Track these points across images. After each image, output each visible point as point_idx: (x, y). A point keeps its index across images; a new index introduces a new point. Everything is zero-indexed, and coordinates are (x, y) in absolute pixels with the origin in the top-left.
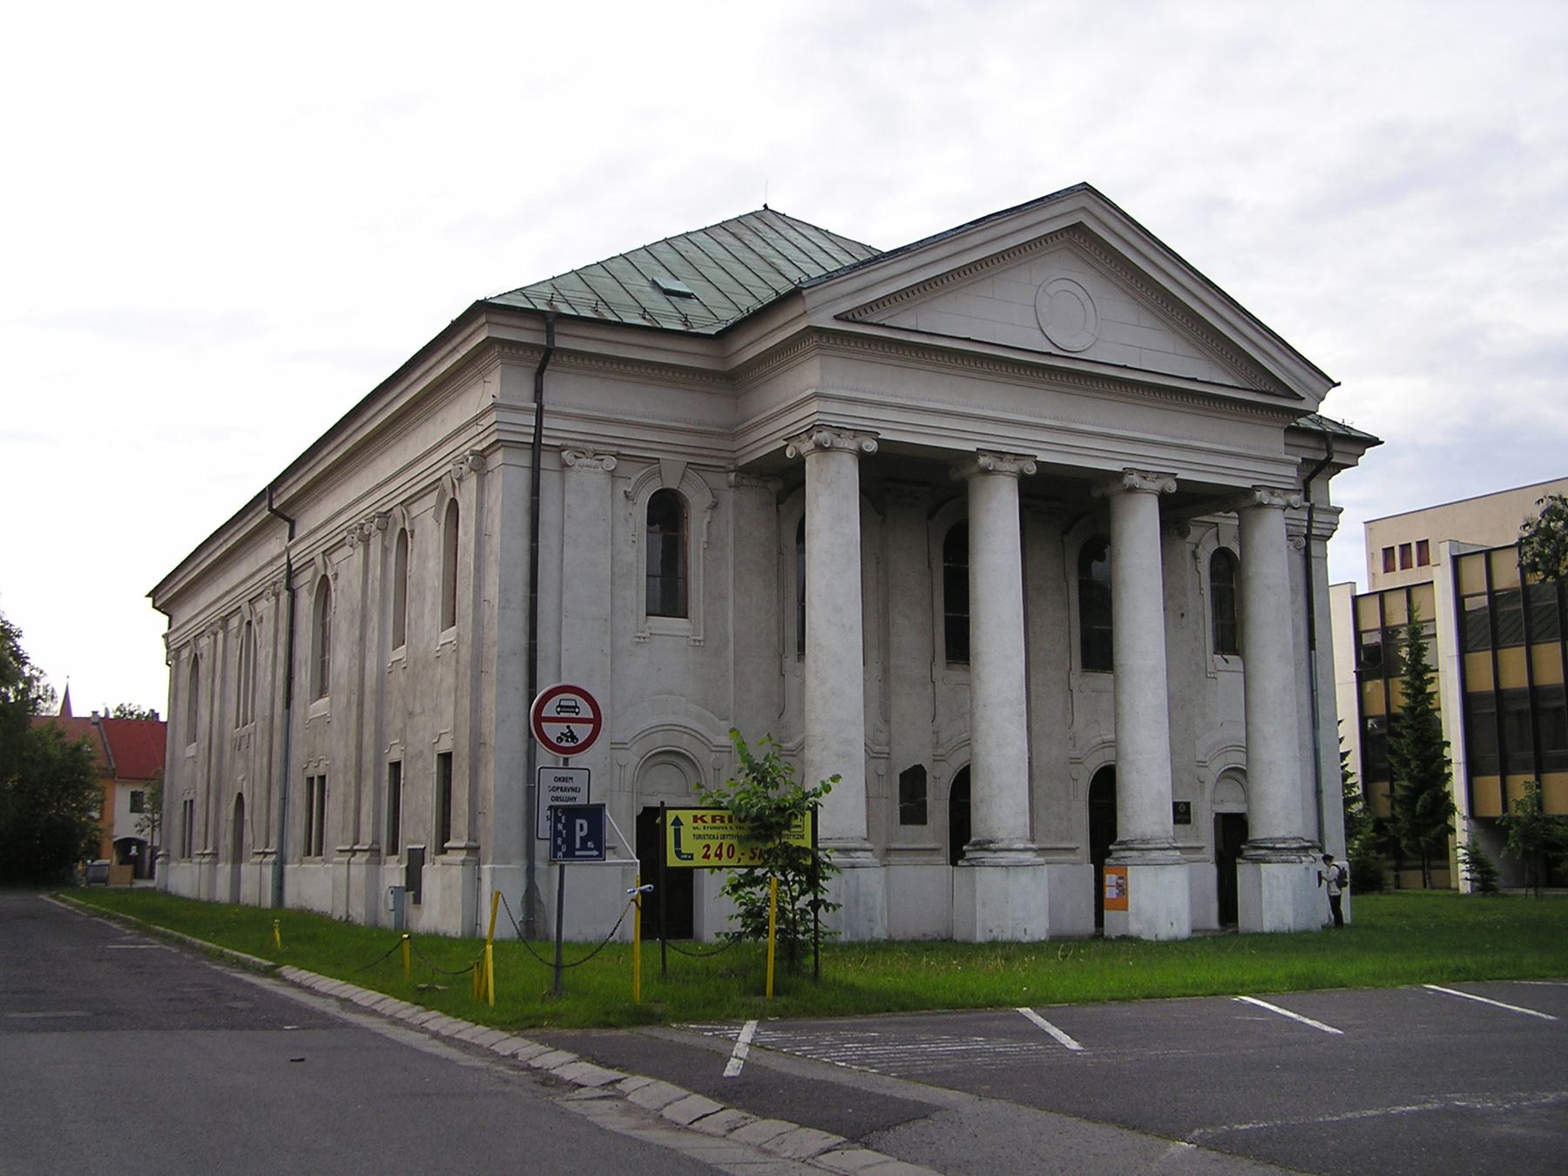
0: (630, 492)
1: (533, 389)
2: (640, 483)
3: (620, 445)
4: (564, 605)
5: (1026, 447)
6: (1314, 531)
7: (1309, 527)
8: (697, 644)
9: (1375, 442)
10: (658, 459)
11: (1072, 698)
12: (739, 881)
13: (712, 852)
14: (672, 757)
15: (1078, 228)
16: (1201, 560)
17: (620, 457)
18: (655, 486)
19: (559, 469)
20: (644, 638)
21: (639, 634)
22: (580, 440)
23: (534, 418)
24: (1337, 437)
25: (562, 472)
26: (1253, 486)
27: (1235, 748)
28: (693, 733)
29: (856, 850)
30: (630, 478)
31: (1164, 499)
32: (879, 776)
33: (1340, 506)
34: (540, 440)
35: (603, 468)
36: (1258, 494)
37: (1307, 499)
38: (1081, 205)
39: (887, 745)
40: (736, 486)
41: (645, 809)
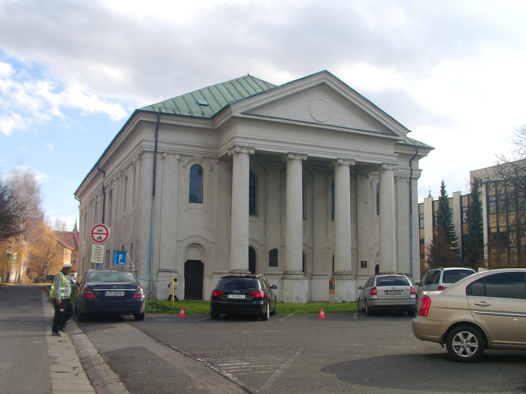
1: (155, 135)
2: (189, 162)
3: (181, 152)
6: (413, 177)
7: (411, 176)
10: (193, 156)
12: (16, 269)
14: (195, 245)
15: (323, 84)
20: (188, 209)
21: (186, 208)
22: (169, 150)
26: (382, 163)
30: (184, 161)
37: (410, 167)
39: (266, 242)
40: (218, 163)
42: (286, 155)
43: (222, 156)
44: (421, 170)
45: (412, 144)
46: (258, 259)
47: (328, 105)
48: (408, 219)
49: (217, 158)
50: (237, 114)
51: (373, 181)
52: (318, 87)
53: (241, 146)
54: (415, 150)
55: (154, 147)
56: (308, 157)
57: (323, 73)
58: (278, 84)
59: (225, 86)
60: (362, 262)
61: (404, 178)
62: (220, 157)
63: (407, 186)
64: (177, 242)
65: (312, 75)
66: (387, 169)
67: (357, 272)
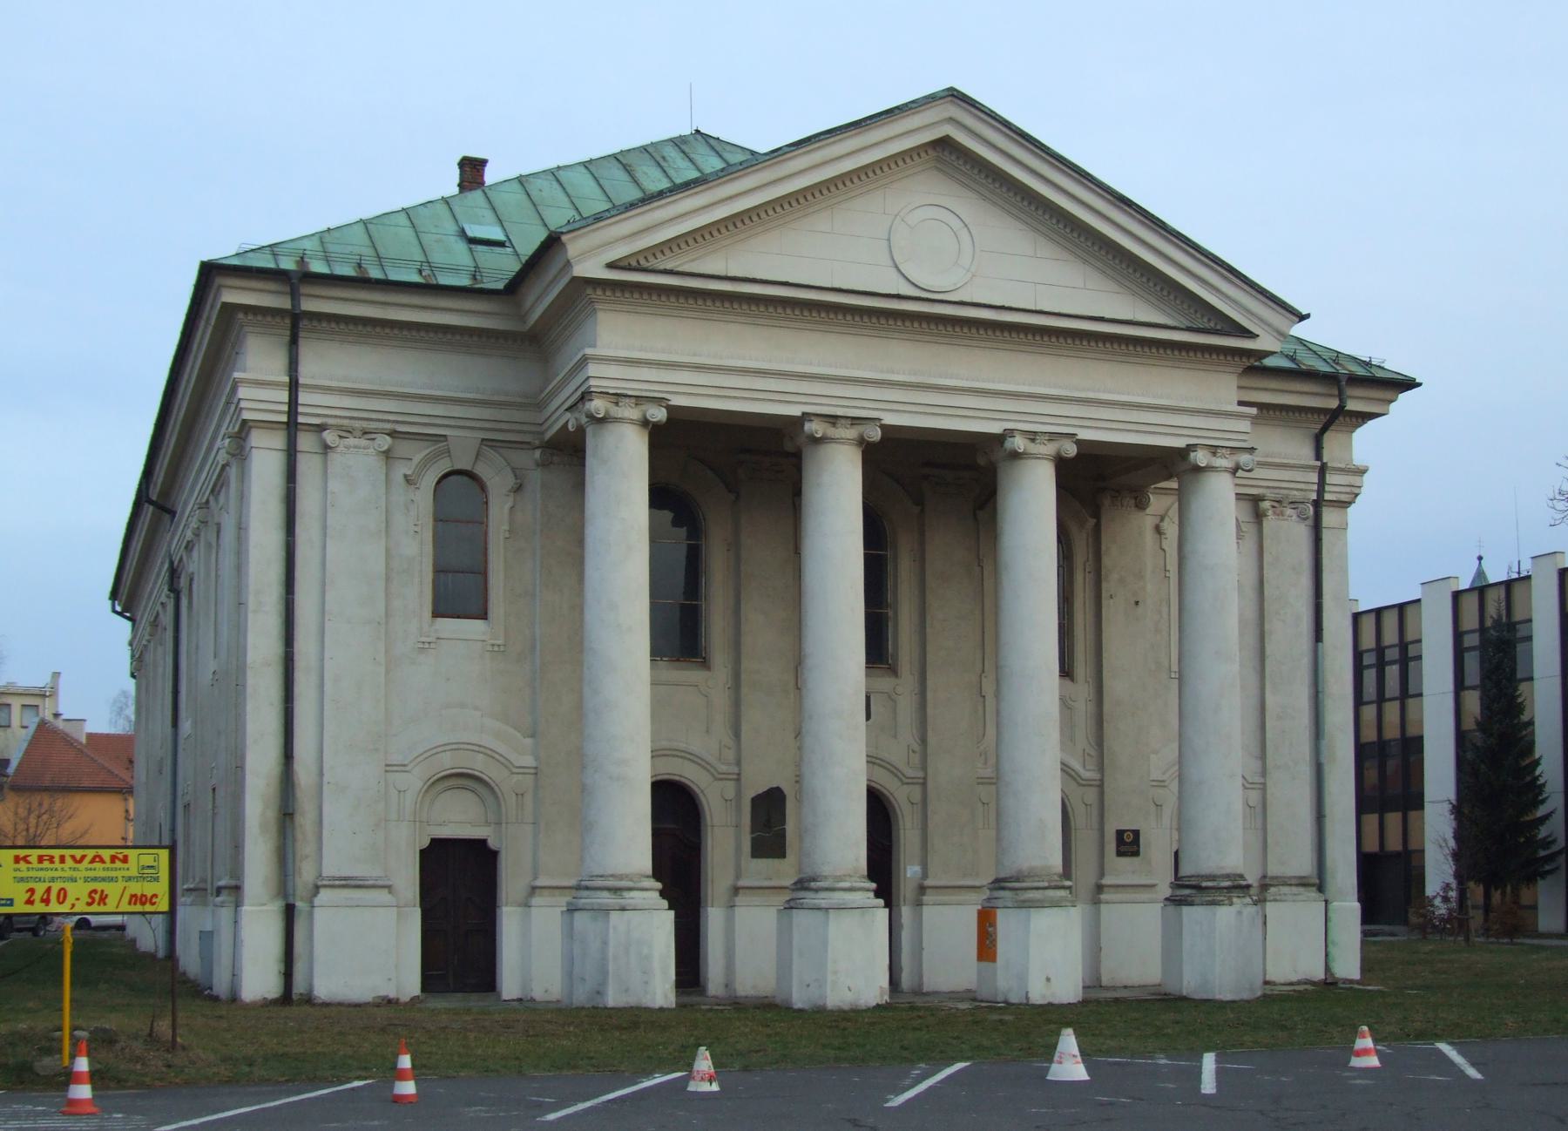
0: (410, 476)
3: (397, 422)
4: (327, 608)
5: (869, 409)
6: (1327, 497)
8: (496, 649)
9: (1408, 384)
10: (445, 436)
11: (984, 706)
13: (37, 897)
14: (465, 779)
15: (944, 144)
16: (1167, 536)
17: (394, 435)
18: (444, 466)
19: (321, 451)
20: (429, 643)
21: (423, 639)
23: (287, 393)
24: (1354, 380)
25: (325, 454)
27: (889, 767)
28: (489, 752)
29: (630, 889)
31: (1064, 467)
32: (726, 800)
33: (1364, 464)
34: (296, 419)
35: (375, 449)
36: (1192, 454)
37: (1318, 456)
38: (946, 115)
40: (543, 464)
41: (434, 841)
42: (798, 422)
43: (554, 435)
44: (1361, 472)
45: (1324, 368)
46: (709, 829)
47: (966, 226)
48: (1305, 662)
49: (537, 442)
50: (591, 268)
51: (1167, 519)
52: (923, 154)
53: (611, 391)
54: (1336, 393)
55: (285, 408)
56: (884, 428)
57: (941, 98)
58: (763, 148)
59: (592, 174)
60: (1120, 834)
61: (1292, 503)
62: (551, 439)
63: (1300, 533)
64: (386, 771)
65: (897, 108)
66: (1209, 469)
67: (1102, 874)
